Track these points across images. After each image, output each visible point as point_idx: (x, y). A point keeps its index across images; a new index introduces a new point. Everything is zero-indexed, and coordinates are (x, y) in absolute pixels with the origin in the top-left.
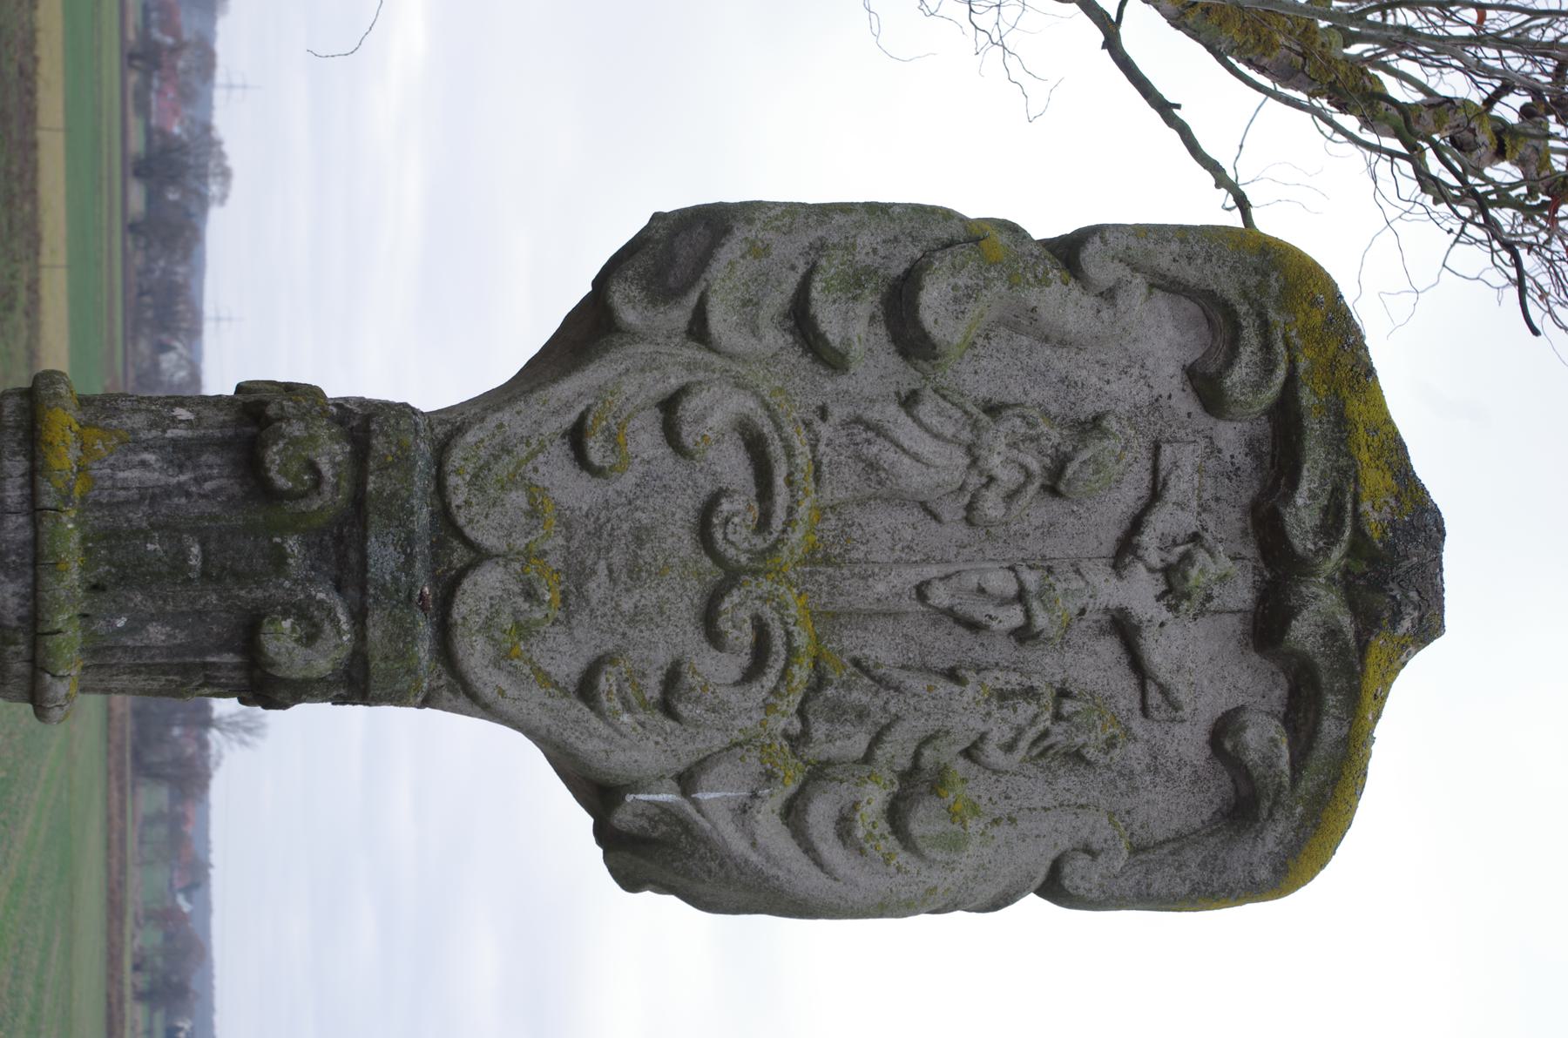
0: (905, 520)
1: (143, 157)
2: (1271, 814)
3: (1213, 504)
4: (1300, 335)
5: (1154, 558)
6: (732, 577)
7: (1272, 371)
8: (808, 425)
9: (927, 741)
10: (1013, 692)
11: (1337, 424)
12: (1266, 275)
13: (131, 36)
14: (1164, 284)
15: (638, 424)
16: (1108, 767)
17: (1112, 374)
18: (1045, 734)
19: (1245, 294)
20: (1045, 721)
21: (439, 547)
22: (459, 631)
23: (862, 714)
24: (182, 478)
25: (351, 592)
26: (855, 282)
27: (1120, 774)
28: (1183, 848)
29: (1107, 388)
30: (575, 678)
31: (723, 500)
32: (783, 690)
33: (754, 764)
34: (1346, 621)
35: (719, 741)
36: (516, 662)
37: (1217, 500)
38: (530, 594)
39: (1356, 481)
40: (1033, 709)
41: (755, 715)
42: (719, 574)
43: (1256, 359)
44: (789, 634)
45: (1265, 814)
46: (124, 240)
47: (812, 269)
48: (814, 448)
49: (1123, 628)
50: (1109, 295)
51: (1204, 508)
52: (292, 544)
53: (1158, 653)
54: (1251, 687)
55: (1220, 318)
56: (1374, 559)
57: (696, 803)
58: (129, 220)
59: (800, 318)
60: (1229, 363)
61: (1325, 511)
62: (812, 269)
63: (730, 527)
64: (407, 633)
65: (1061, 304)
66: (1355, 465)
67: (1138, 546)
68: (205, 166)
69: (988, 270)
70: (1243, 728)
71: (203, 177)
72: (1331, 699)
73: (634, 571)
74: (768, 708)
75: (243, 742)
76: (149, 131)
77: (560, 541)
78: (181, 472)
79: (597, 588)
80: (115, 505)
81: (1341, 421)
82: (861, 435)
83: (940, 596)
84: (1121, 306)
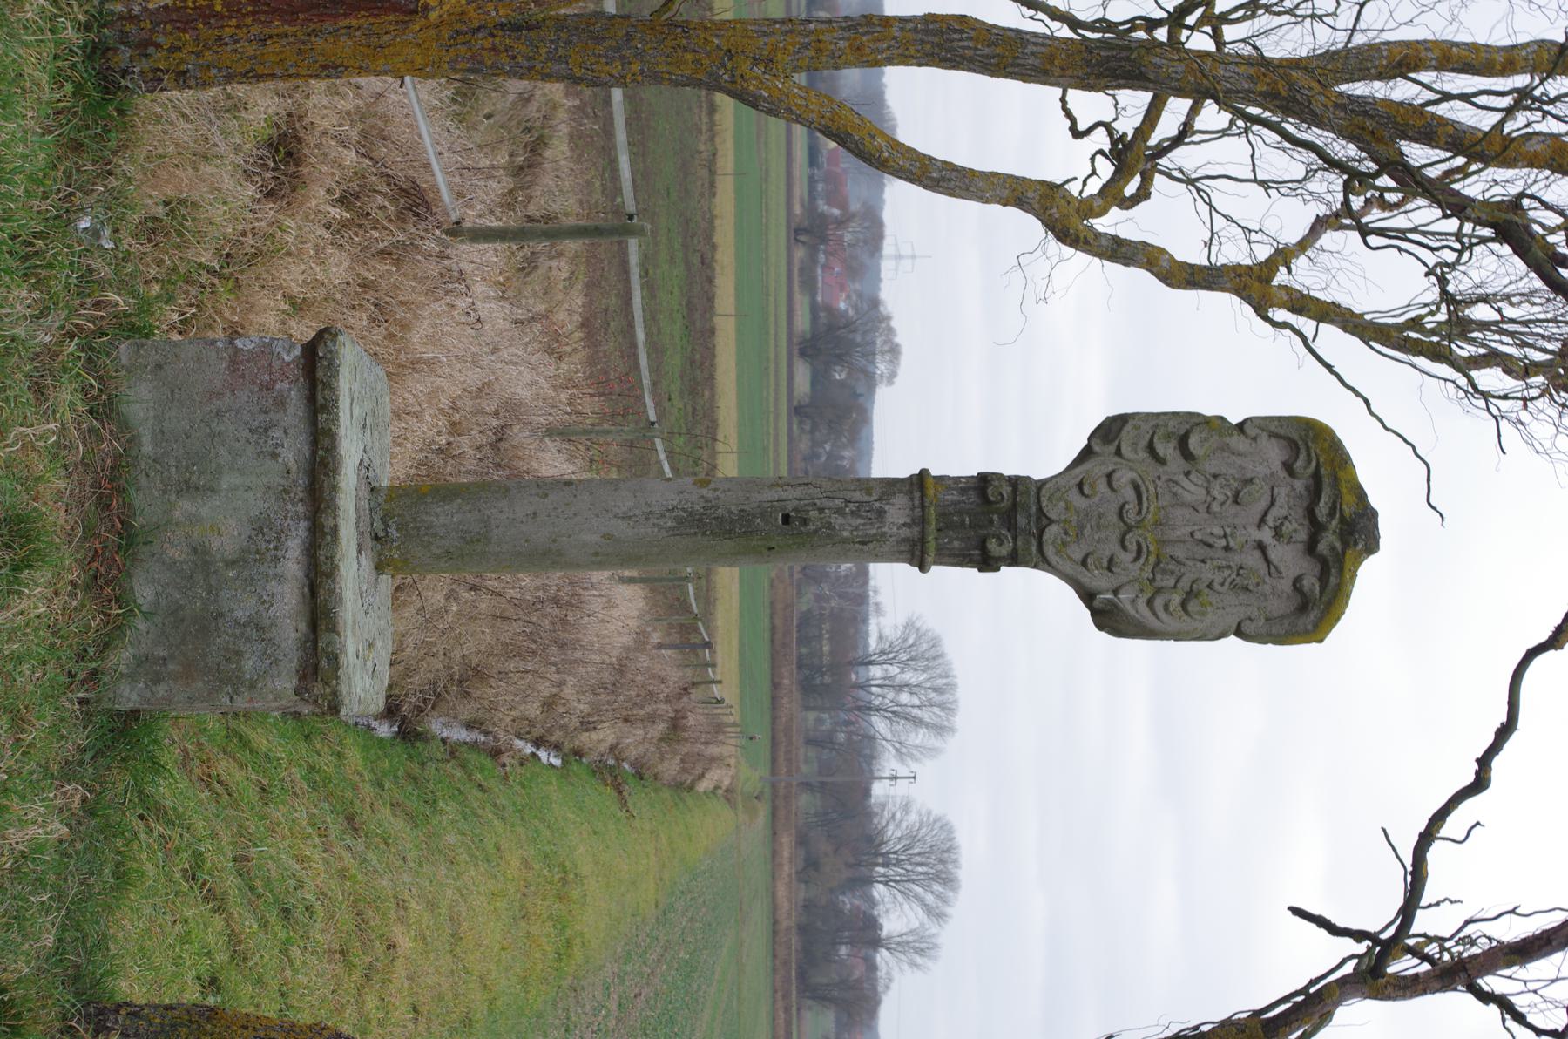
0: (1187, 512)
1: (808, 336)
6: (1130, 528)
13: (797, 209)
14: (1273, 435)
21: (1038, 519)
23: (1172, 573)
26: (1168, 436)
34: (1338, 545)
35: (1126, 580)
38: (1066, 533)
46: (790, 424)
49: (1261, 547)
50: (1254, 439)
52: (995, 517)
53: (1272, 556)
55: (1293, 446)
56: (1348, 524)
58: (795, 403)
59: (1151, 448)
64: (1028, 543)
65: (1239, 443)
68: (873, 343)
71: (870, 355)
75: (913, 964)
76: (814, 309)
79: (1087, 531)
81: (1336, 480)
83: (1198, 536)
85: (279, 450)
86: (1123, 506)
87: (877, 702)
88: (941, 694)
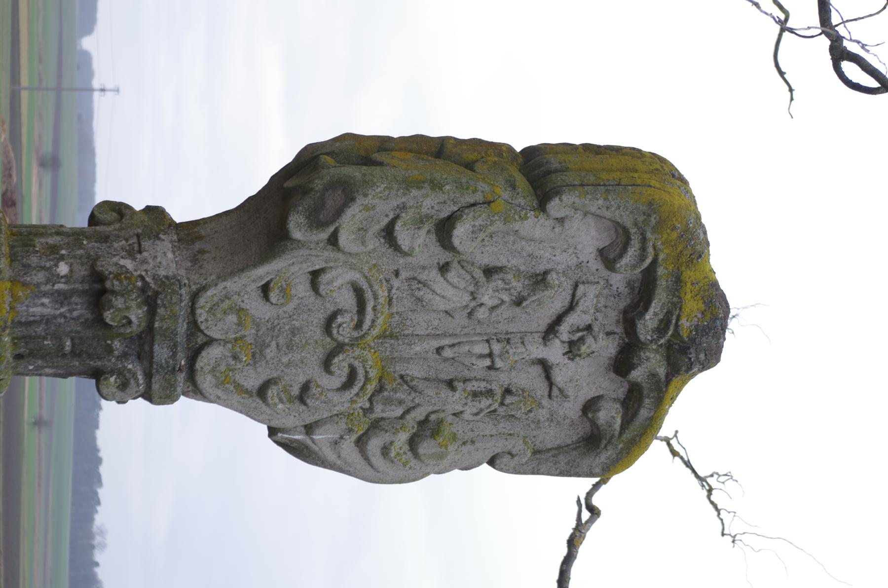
2: (606, 447)
3: (603, 309)
4: (662, 244)
5: (565, 337)
6: (339, 348)
7: (644, 260)
8: (388, 281)
9: (434, 412)
10: (481, 392)
11: (676, 282)
12: (649, 216)
15: (298, 281)
16: (527, 419)
17: (558, 252)
18: (495, 411)
19: (636, 224)
20: (496, 405)
22: (199, 373)
23: (401, 402)
24: (62, 310)
25: (145, 362)
27: (533, 422)
28: (559, 454)
29: (554, 258)
30: (257, 387)
31: (339, 317)
32: (361, 395)
33: (343, 425)
35: (326, 415)
36: (227, 386)
37: (606, 307)
39: (680, 309)
40: (490, 401)
41: (345, 405)
42: (334, 344)
43: (636, 253)
44: (366, 372)
45: (603, 446)
47: (397, 217)
48: (390, 291)
49: (545, 366)
51: (597, 310)
53: (559, 377)
54: (612, 388)
57: (313, 441)
60: (621, 256)
61: (661, 321)
62: (397, 217)
63: (341, 329)
66: (681, 302)
67: (557, 332)
69: (493, 216)
70: (599, 410)
72: (647, 401)
73: (290, 347)
74: (352, 401)
77: (253, 331)
78: (62, 307)
79: (271, 352)
80: (29, 324)
81: (678, 281)
82: (415, 285)
84: (566, 226)
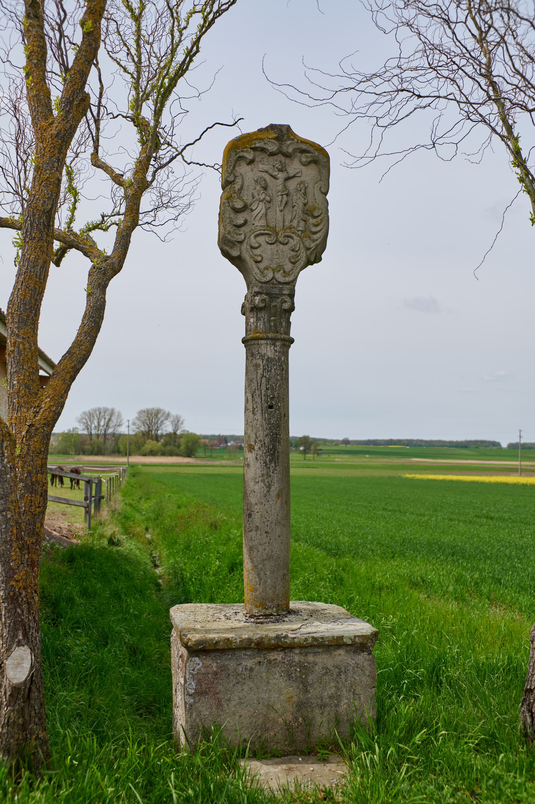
75: (182, 423)
85: (249, 668)
86: (268, 243)
87: (103, 432)
88: (100, 413)
